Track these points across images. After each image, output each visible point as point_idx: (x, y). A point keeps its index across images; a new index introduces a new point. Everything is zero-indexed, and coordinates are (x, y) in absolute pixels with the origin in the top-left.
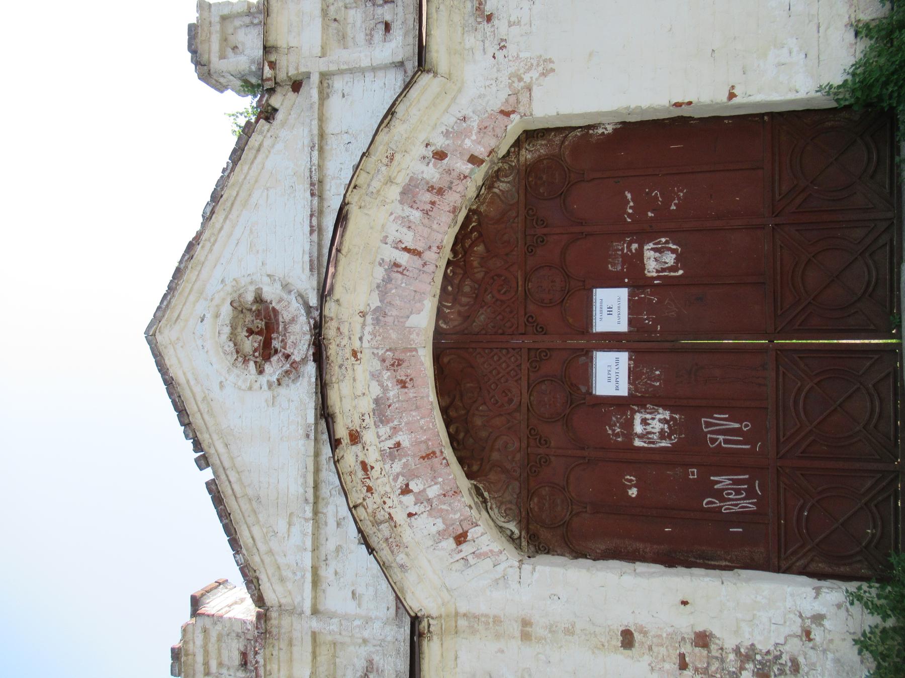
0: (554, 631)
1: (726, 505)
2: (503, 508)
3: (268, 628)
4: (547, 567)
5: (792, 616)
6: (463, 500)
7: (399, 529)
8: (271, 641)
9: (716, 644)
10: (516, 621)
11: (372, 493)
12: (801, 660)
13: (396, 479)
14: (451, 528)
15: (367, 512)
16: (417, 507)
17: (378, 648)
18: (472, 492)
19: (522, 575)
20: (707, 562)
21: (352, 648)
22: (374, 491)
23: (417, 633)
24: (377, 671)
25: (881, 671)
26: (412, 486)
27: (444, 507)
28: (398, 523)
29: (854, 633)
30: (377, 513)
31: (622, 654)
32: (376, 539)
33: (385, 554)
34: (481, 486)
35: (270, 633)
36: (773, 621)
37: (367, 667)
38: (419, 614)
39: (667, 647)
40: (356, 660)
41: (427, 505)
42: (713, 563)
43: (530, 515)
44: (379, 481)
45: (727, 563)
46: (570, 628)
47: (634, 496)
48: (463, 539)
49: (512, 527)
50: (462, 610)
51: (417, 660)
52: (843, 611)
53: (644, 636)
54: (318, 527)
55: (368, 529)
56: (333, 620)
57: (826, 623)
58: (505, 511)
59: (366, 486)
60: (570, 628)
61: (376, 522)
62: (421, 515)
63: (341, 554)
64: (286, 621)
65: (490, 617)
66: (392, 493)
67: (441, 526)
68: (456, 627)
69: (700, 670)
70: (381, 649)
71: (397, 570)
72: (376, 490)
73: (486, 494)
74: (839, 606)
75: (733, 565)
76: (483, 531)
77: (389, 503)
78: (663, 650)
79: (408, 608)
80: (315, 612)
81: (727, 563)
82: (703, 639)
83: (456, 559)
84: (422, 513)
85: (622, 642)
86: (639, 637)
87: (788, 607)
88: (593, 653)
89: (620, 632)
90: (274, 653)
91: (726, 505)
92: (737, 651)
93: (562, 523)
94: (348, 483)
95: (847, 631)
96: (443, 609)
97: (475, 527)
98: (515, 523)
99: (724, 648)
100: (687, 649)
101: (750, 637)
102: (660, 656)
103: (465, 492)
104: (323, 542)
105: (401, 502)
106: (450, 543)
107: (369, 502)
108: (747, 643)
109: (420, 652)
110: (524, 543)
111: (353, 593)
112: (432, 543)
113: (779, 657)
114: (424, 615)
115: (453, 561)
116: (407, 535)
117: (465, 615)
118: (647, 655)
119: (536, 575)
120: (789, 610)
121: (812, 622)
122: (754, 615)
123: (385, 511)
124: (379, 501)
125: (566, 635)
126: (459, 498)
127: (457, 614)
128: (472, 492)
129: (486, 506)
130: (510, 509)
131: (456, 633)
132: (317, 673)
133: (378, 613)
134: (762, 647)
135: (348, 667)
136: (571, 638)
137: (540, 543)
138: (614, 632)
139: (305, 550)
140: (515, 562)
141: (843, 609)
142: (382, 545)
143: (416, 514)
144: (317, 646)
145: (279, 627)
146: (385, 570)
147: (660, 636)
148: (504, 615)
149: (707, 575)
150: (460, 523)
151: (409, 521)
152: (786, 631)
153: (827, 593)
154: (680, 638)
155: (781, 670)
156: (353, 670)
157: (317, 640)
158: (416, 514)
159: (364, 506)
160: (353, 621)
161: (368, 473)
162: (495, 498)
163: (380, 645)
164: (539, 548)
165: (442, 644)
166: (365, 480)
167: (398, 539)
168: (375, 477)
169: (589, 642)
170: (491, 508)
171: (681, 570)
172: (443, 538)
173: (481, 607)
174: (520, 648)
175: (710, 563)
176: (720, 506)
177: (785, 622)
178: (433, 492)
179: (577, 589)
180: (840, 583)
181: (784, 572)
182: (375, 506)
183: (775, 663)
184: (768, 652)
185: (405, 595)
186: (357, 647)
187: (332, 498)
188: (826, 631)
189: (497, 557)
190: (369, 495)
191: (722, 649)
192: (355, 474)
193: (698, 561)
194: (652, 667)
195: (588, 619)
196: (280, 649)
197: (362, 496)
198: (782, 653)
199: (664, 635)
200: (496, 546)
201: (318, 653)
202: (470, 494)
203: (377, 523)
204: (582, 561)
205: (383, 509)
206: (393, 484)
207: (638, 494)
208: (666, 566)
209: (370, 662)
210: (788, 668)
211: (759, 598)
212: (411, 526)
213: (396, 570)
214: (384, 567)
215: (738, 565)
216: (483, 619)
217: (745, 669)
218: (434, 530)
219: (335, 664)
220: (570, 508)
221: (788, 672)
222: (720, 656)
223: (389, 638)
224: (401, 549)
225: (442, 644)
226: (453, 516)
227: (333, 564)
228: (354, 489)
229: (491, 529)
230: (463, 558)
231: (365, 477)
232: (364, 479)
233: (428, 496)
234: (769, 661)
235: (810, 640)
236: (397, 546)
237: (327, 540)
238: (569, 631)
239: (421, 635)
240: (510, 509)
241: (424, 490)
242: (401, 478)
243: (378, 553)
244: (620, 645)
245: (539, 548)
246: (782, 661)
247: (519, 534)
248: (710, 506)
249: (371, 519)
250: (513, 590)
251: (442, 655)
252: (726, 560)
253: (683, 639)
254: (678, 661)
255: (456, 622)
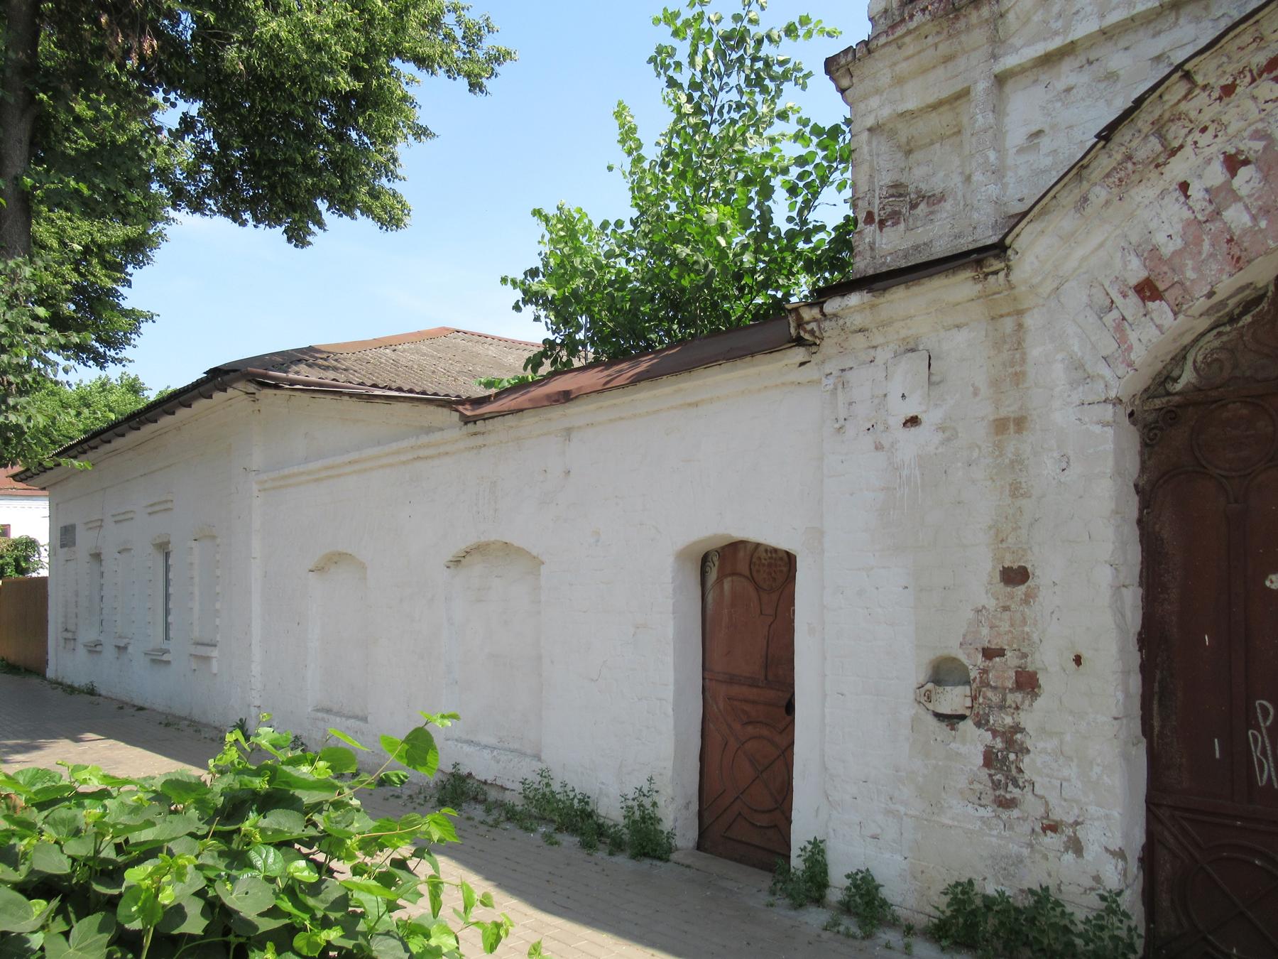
0: (1013, 467)
1: (1263, 737)
2: (1223, 356)
3: (963, 11)
4: (1112, 446)
5: (1076, 811)
6: (1224, 277)
7: (1154, 175)
8: (945, 25)
9: (1023, 702)
10: (1021, 409)
11: (1220, 99)
12: (1015, 813)
13: (1257, 135)
14: (1165, 269)
15: (1179, 101)
16: (1202, 194)
17: (962, 203)
18: (1248, 292)
19: (1096, 406)
20: (1156, 697)
21: (957, 162)
22: (1226, 100)
23: (981, 256)
24: (932, 213)
25: (1013, 912)
26: (1244, 173)
27: (1206, 247)
28: (1166, 170)
29: (1060, 890)
30: (1180, 123)
31: (994, 568)
32: (1128, 138)
33: (1104, 162)
34: (1264, 305)
35: (957, 18)
36: (1064, 784)
37: (934, 195)
38: (1010, 252)
39: (1010, 631)
40: (941, 174)
41: (1207, 212)
42: (1155, 707)
43: (1214, 406)
44: (1250, 104)
45: (1156, 730)
46: (1021, 491)
47: (1268, 583)
48: (1148, 294)
49: (1187, 377)
50: (1028, 321)
51: (938, 268)
52: (1089, 883)
53: (1021, 599)
54: (1150, 22)
55: (1144, 120)
56: (991, 114)
57: (1070, 857)
58: (1217, 360)
59: (1235, 79)
60: (1021, 491)
61: (1162, 127)
62: (1185, 208)
63: (1102, 86)
64: (979, 36)
65: (1021, 366)
66: (1225, 138)
67: (1168, 249)
68: (1002, 316)
69: (985, 676)
70: (961, 208)
71: (1076, 193)
72: (1228, 104)
73: (1248, 319)
74: (1097, 879)
75: (1155, 739)
76: (1166, 327)
77: (1207, 138)
78: (1005, 626)
79: (1017, 230)
80: (1001, 80)
81: (1156, 730)
82: (1027, 683)
83: (1109, 290)
84: (1190, 208)
85: (1010, 569)
86: (1019, 593)
87: (1089, 808)
88: (990, 528)
89: (1023, 565)
90: (930, 38)
91: (1263, 737)
92: (1017, 729)
93: (1204, 463)
94: (1238, 42)
95: (1061, 882)
96: (1023, 289)
97: (1172, 310)
98: (1193, 381)
99: (1019, 711)
100: (1011, 659)
101: (1038, 749)
102: (997, 623)
103: (1242, 278)
104: (1122, 44)
105: (1209, 161)
106: (1136, 271)
107: (1201, 99)
108: (1029, 743)
109: (955, 270)
110: (1158, 403)
111: (1039, 133)
112: (1133, 241)
113: (1016, 785)
114: (1009, 260)
115: (1106, 287)
116: (1144, 194)
117: (1020, 326)
118: (997, 604)
119: (1097, 429)
120: (1084, 809)
121: (1069, 837)
122: (1070, 758)
123: (1186, 136)
124: (1205, 118)
125: (1011, 485)
126: (1227, 269)
127: (1020, 313)
128: (1248, 292)
129: (1224, 324)
130: (1221, 369)
131: (993, 319)
132: (915, 121)
133: (1011, 185)
134: (1026, 762)
135: (931, 166)
136: (1007, 492)
137: (1161, 429)
138: (1023, 556)
139: (1103, 16)
140: (1115, 390)
141: (1094, 884)
142: (1117, 152)
143: (1187, 197)
144: (951, 104)
145: (969, 29)
146: (1074, 171)
147: (1024, 622)
148: (1028, 388)
149: (1127, 695)
150: (1176, 282)
151: (1171, 189)
152: (1053, 799)
153: (1116, 868)
154: (1024, 650)
155: (999, 784)
156: (928, 175)
157: (959, 102)
158: (1187, 197)
159: (1190, 92)
160: (994, 149)
161: (1265, 75)
162: (1242, 336)
163: (966, 205)
164: (1153, 428)
165: (973, 300)
166: (1248, 75)
167: (1136, 177)
168: (1256, 92)
169: (1004, 520)
170: (1220, 334)
171: (1135, 659)
172: (1145, 259)
173: (1036, 351)
174: (983, 419)
175: (1155, 702)
176: (1260, 727)
177: (1065, 800)
178: (1237, 217)
179: (1081, 497)
180: (1138, 886)
181: (1148, 810)
182: (1193, 114)
183: (1007, 778)
184: (1020, 771)
185: (1037, 220)
186: (960, 170)
187: (1210, 24)
188: (1059, 854)
189: (1121, 359)
190: (1216, 94)
191: (1017, 708)
192: (1259, 49)
193: (1156, 685)
194: (981, 611)
195: (1037, 516)
196: (936, 46)
197: (1212, 81)
198: (1022, 788)
199: (1027, 629)
200: (1139, 354)
201: (941, 110)
202: (1242, 289)
203: (1159, 129)
204: (1133, 503)
205: (1190, 132)
206: (1245, 134)
207: (1273, 590)
208: (1140, 634)
209: (942, 198)
210: (1003, 793)
211: (1097, 769)
212: (1162, 195)
213: (1076, 191)
214: (1079, 169)
215: (1155, 745)
216: (1018, 356)
217: (994, 737)
218: (1160, 238)
219: (932, 143)
220: (1234, 474)
221: (997, 793)
222: (1007, 704)
223: (975, 215)
224: (1115, 190)
225: (973, 300)
226: (1190, 266)
227: (1083, 79)
228: (1225, 59)
229: (1175, 340)
230: (1112, 302)
231: (1255, 72)
232: (1251, 71)
233: (1226, 208)
234: (1009, 770)
235: (1044, 829)
236: (1120, 180)
237: (1126, 49)
238: (1016, 491)
239: (979, 263)
240: (1221, 369)
241: (1237, 198)
242: (1259, 145)
243: (1103, 151)
244: (1006, 566)
245: (1153, 428)
246: (1011, 787)
247: (1174, 391)
248: (1259, 710)
249: (1167, 116)
250: (1069, 396)
251: (958, 304)
252: (1163, 727)
253: (1025, 656)
254: (993, 647)
255: (1009, 314)
